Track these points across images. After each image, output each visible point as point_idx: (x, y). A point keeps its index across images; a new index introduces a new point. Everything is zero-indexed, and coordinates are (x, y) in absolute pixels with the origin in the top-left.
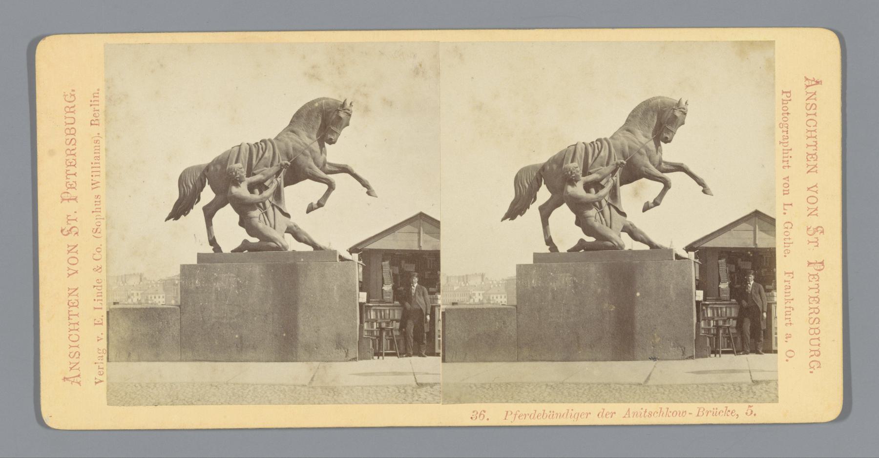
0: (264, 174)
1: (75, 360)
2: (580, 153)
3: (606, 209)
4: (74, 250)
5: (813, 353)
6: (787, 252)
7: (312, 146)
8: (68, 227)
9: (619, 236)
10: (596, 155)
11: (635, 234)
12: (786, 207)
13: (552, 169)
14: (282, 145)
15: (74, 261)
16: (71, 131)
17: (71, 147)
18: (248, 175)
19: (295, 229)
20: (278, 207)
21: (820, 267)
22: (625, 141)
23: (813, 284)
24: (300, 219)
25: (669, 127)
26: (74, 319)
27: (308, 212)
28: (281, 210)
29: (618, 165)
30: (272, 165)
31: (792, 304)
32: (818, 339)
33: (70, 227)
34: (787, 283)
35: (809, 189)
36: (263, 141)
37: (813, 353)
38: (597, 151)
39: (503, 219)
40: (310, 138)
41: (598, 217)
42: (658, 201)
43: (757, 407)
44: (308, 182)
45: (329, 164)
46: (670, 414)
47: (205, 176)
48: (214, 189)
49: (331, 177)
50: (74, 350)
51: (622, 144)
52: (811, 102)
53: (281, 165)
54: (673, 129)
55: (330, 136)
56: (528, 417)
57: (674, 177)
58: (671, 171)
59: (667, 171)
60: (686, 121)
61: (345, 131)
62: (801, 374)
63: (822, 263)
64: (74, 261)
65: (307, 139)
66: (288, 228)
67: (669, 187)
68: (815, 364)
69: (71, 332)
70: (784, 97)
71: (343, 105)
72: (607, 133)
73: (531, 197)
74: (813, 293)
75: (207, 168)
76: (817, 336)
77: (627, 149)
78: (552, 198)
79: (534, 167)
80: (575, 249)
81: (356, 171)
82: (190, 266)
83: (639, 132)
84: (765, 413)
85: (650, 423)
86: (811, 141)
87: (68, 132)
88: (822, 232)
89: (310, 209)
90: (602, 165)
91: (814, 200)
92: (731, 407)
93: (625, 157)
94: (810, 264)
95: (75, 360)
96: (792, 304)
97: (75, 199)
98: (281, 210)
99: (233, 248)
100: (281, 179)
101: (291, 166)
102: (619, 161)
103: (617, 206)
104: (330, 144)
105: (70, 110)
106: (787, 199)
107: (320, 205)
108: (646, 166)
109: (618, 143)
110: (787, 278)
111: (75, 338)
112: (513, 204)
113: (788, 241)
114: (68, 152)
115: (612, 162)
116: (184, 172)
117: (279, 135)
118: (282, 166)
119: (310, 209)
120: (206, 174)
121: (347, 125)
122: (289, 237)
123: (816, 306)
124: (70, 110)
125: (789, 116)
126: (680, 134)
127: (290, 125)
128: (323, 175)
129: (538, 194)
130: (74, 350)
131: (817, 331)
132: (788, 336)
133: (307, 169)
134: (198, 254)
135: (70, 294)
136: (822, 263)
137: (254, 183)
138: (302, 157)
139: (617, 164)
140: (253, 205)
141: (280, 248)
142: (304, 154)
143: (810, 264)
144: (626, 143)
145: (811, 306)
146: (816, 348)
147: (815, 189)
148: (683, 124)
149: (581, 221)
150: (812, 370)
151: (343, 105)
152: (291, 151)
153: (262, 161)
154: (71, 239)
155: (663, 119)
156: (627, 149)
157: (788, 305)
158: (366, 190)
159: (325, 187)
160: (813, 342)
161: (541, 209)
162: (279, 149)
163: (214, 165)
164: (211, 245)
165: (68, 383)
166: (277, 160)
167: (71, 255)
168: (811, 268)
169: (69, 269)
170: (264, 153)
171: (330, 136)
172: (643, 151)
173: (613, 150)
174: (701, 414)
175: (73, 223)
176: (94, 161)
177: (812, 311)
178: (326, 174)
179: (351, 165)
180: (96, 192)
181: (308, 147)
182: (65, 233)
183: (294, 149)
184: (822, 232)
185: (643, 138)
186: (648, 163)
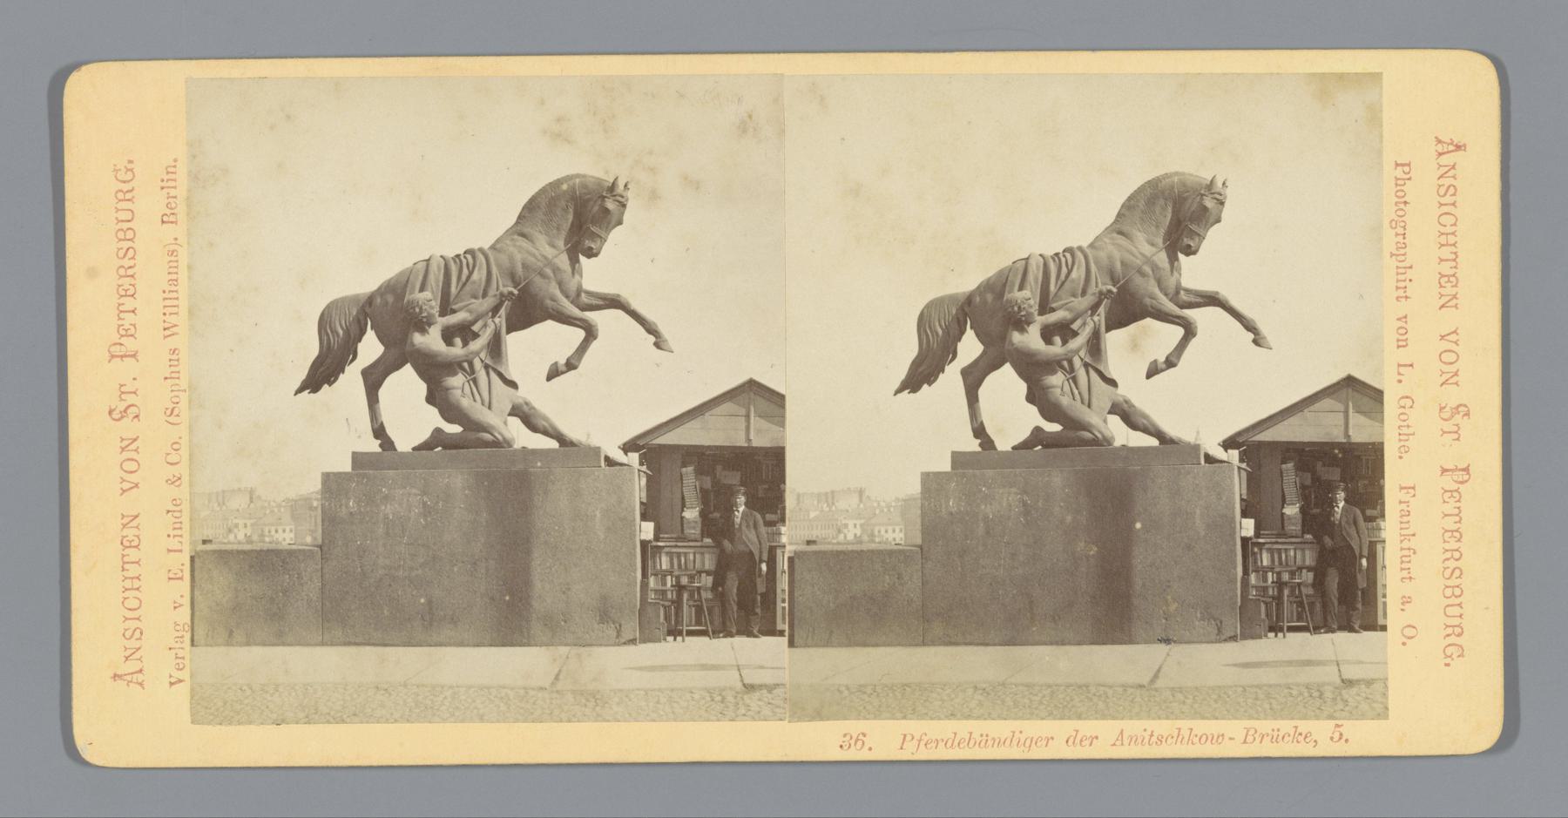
0: (470, 312)
1: (134, 644)
2: (1035, 273)
3: (1081, 373)
4: (133, 447)
5: (1450, 631)
6: (1404, 450)
7: (556, 261)
8: (122, 406)
9: (1105, 421)
10: (1063, 277)
11: (1133, 418)
12: (1402, 370)
13: (985, 302)
14: (504, 258)
15: (131, 466)
16: (126, 235)
17: (127, 263)
18: (443, 313)
19: (526, 408)
20: (495, 371)
21: (1462, 476)
22: (1114, 251)
23: (1450, 508)
24: (534, 391)
25: (1194, 227)
26: (133, 570)
27: (549, 379)
28: (501, 375)
29: (1102, 296)
30: (485, 295)
31: (1413, 543)
32: (1460, 605)
33: (124, 405)
34: (1403, 506)
35: (1442, 337)
36: (470, 252)
37: (1450, 631)
38: (1064, 270)
39: (898, 392)
40: (553, 246)
41: (1067, 388)
42: (1174, 359)
43: (1350, 727)
44: (550, 325)
45: (587, 293)
46: (1196, 740)
47: (366, 315)
48: (381, 338)
49: (591, 316)
50: (133, 624)
51: (1110, 258)
52: (1447, 182)
53: (502, 295)
54: (1200, 231)
55: (588, 243)
56: (941, 745)
57: (1202, 317)
58: (1198, 305)
59: (1191, 306)
60: (1224, 215)
61: (616, 235)
62: (1429, 668)
63: (1466, 470)
64: (131, 466)
65: (548, 248)
66: (514, 408)
67: (1194, 335)
68: (1454, 650)
69: (127, 594)
70: (1399, 172)
71: (612, 188)
72: (1082, 237)
73: (948, 351)
74: (1450, 523)
75: (370, 300)
76: (1457, 601)
77: (1118, 265)
78: (984, 353)
79: (952, 298)
80: (1026, 445)
81: (635, 305)
82: (339, 476)
83: (1140, 236)
84: (1365, 738)
85: (1159, 756)
86: (1446, 253)
87: (121, 235)
88: (1467, 414)
89: (554, 373)
90: (1074, 296)
91: (1452, 357)
92: (1304, 726)
93: (1114, 281)
94: (1444, 471)
95: (134, 644)
96: (1413, 543)
97: (134, 356)
98: (501, 375)
99: (416, 444)
100: (501, 320)
101: (519, 297)
102: (1104, 288)
103: (1101, 368)
104: (589, 256)
105: (126, 196)
106: (1404, 356)
107: (571, 366)
108: (1152, 297)
109: (1102, 255)
110: (1403, 496)
111: (133, 603)
112: (916, 364)
113: (1405, 430)
114: (122, 272)
115: (1092, 289)
116: (328, 307)
117: (498, 241)
118: (503, 297)
119: (554, 373)
120: (368, 310)
121: (620, 223)
122: (515, 422)
123: (1456, 546)
124: (126, 196)
125: (1407, 208)
126: (1214, 239)
127: (517, 223)
128: (576, 312)
129: (960, 346)
130: (133, 624)
131: (1457, 591)
132: (1406, 600)
133: (548, 302)
134: (354, 454)
135: (124, 526)
136: (1466, 470)
137: (454, 326)
138: (538, 280)
139: (1101, 293)
140: (452, 367)
141: (500, 444)
142: (542, 275)
143: (1444, 471)
144: (1117, 255)
145: (1447, 546)
146: (1456, 621)
147: (1453, 337)
148: (1218, 221)
149: (1037, 395)
150: (1448, 660)
151: (612, 188)
152: (519, 270)
153: (468, 288)
154: (127, 427)
155: (1182, 213)
156: (1118, 265)
157: (1406, 544)
158: (652, 339)
159: (580, 334)
160: (1450, 611)
161: (965, 373)
162: (498, 266)
163: (382, 295)
164: (376, 437)
165: (121, 684)
166: (494, 285)
167: (127, 455)
168: (1447, 478)
169: (123, 480)
170: (471, 273)
171: (588, 243)
172: (1147, 269)
173: (1093, 268)
174: (1250, 739)
175: (131, 399)
176: (167, 288)
177: (1448, 555)
178: (581, 311)
179: (627, 295)
180: (172, 343)
181: (549, 263)
182: (116, 416)
183: (524, 266)
184: (1467, 414)
185: (1146, 246)
186: (1157, 291)
